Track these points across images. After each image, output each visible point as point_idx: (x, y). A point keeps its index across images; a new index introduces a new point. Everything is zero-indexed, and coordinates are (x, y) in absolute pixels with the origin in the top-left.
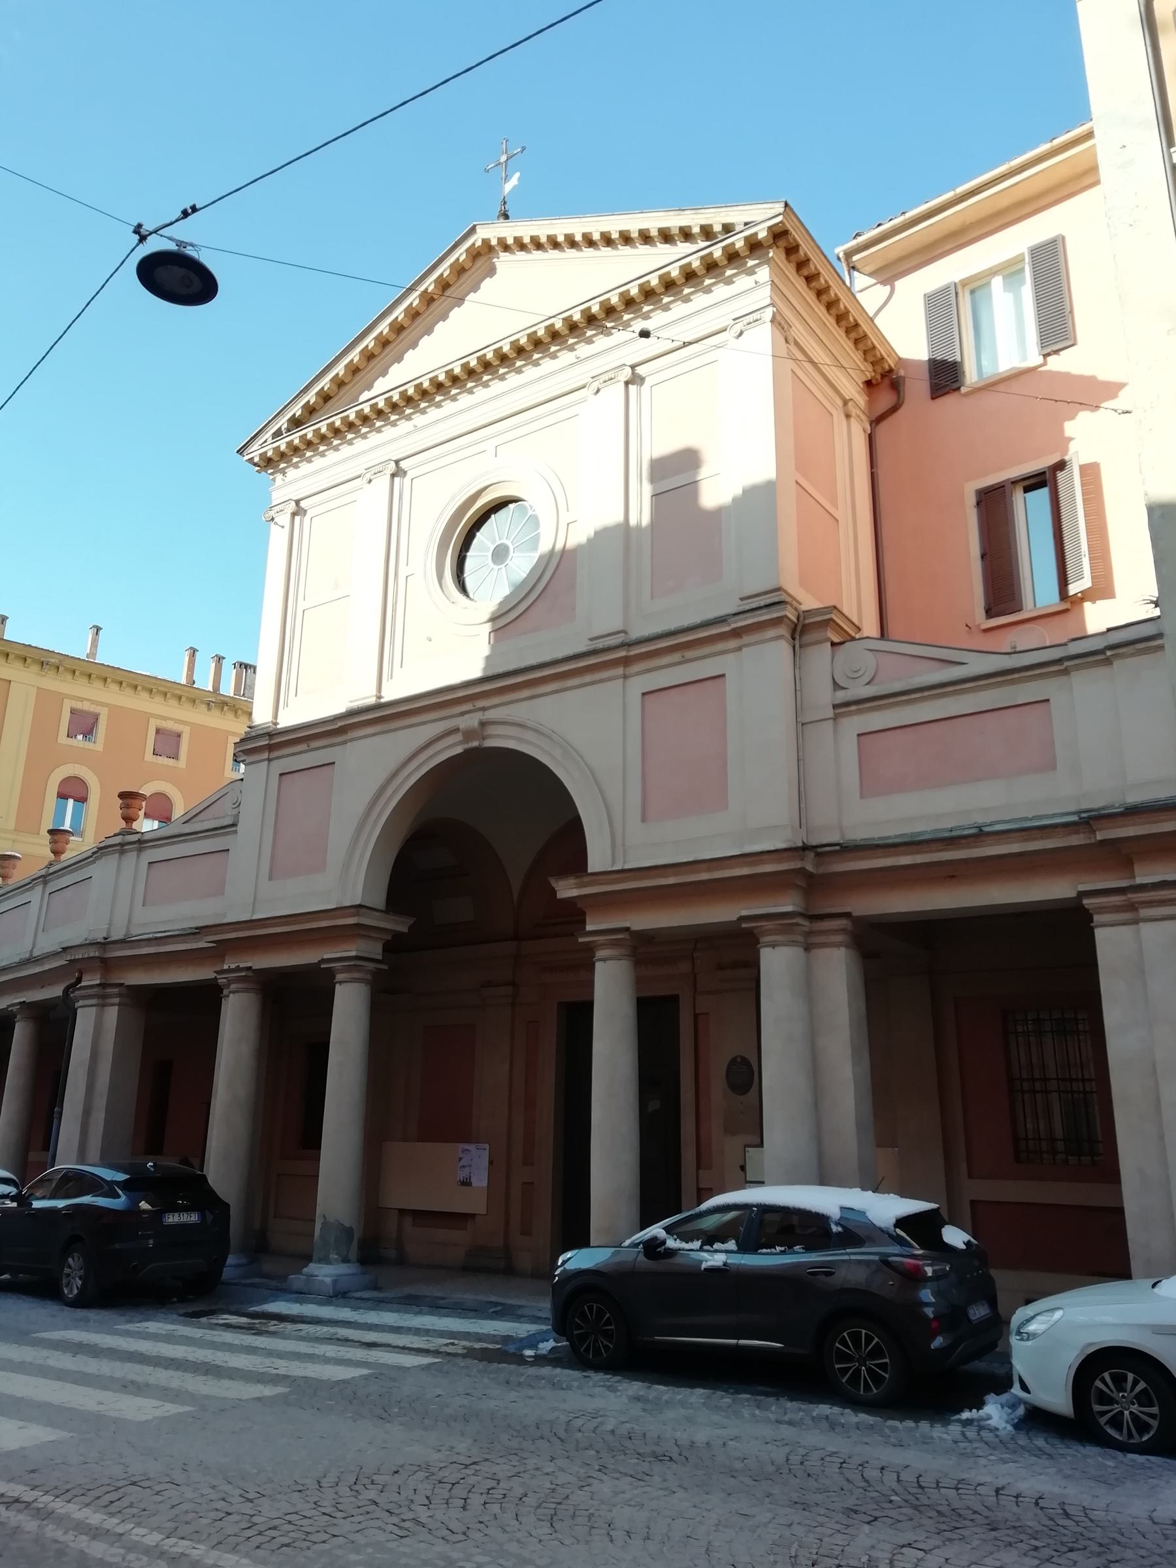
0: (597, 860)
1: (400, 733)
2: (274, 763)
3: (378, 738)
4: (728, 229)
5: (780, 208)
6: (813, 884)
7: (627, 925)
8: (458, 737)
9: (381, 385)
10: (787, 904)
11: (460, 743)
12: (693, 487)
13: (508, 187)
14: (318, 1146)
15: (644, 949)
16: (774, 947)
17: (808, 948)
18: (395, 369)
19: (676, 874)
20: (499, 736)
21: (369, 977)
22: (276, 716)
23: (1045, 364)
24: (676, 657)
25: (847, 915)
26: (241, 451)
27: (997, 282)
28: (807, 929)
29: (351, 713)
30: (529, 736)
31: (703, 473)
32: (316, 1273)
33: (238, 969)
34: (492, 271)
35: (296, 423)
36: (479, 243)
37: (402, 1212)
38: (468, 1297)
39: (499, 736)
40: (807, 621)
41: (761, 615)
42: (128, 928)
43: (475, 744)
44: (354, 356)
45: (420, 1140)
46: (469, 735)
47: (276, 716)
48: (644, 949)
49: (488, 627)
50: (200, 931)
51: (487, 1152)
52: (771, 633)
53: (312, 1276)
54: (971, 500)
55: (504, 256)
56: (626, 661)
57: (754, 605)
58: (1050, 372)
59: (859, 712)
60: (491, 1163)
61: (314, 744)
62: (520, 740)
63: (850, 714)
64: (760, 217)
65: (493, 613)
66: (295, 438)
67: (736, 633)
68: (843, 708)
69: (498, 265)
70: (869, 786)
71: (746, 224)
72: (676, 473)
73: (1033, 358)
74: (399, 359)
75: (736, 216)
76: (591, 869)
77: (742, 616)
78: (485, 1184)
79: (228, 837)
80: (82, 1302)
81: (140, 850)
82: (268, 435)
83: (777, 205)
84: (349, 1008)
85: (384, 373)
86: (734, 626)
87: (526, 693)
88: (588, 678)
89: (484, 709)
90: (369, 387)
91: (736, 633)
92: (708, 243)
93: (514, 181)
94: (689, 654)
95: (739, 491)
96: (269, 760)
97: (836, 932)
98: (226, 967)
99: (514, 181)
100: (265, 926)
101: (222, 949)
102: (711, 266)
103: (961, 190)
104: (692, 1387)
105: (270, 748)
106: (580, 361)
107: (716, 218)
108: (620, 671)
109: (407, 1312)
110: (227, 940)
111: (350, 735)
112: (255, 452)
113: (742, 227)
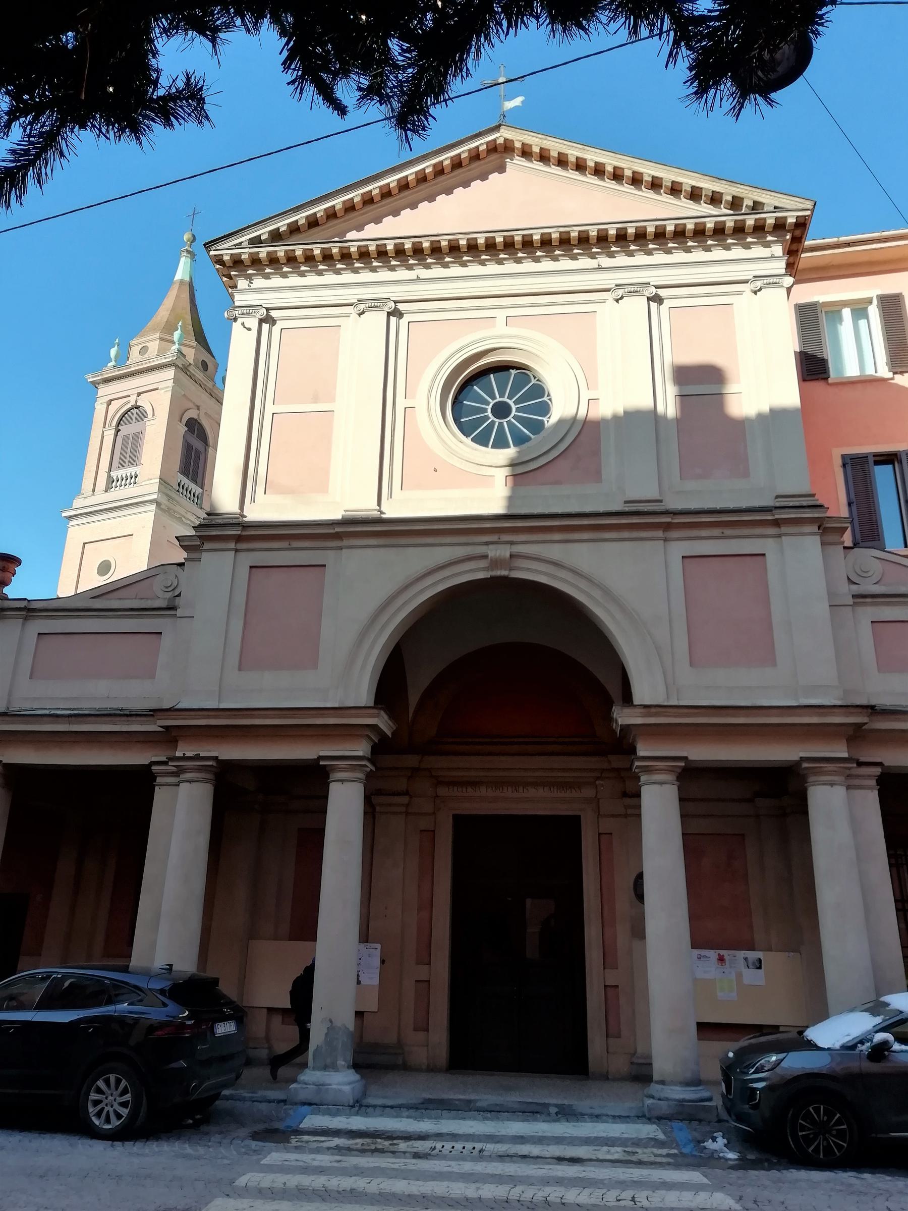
0: (642, 693)
1: (411, 549)
2: (242, 555)
3: (382, 550)
4: (757, 206)
5: (809, 205)
6: (856, 735)
7: (684, 754)
8: (483, 564)
9: (372, 231)
10: (841, 751)
11: (484, 569)
12: (719, 398)
13: (509, 105)
14: (130, 943)
15: (690, 776)
16: (832, 785)
17: (848, 787)
18: (388, 220)
19: (747, 716)
20: (528, 569)
21: (210, 776)
22: (242, 506)
23: (892, 379)
24: (717, 532)
25: (880, 764)
26: (208, 245)
27: (846, 313)
28: (849, 771)
29: (347, 522)
30: (562, 574)
31: (731, 388)
32: (328, 1082)
33: (197, 758)
34: (501, 169)
35: (276, 237)
36: (501, 141)
37: (271, 1010)
38: (487, 1098)
39: (528, 569)
40: (828, 525)
41: (804, 513)
42: (9, 702)
43: (504, 573)
44: (355, 195)
45: (291, 939)
46: (496, 563)
47: (242, 506)
48: (690, 776)
49: (506, 471)
50: (154, 713)
51: (378, 952)
52: (808, 529)
53: (323, 1085)
54: (838, 462)
55: (519, 160)
56: (667, 527)
57: (797, 504)
58: (897, 385)
59: (872, 604)
60: (383, 962)
61: (296, 544)
62: (555, 577)
63: (865, 604)
64: (793, 209)
65: (513, 459)
66: (280, 251)
67: (777, 523)
68: (861, 598)
69: (509, 166)
70: (885, 663)
71: (775, 208)
72: (700, 383)
73: (884, 372)
74: (396, 213)
75: (768, 199)
76: (635, 703)
77: (787, 510)
78: (376, 981)
79: (69, 620)
80: (125, 1134)
81: (26, 619)
82: (244, 238)
83: (808, 202)
84: (345, 805)
85: (378, 220)
86: (777, 516)
87: (557, 536)
88: (626, 534)
89: (512, 543)
90: (360, 228)
91: (777, 523)
92: (731, 212)
93: (518, 101)
94: (728, 532)
95: (766, 409)
96: (237, 551)
97: (870, 777)
98: (179, 754)
99: (518, 101)
100: (252, 717)
101: (170, 737)
102: (739, 230)
103: (842, 239)
104: (846, 1171)
105: (239, 539)
106: (600, 268)
107: (750, 195)
108: (660, 534)
109: (464, 1119)
110: (172, 729)
111: (346, 542)
112: (226, 251)
113: (772, 209)
